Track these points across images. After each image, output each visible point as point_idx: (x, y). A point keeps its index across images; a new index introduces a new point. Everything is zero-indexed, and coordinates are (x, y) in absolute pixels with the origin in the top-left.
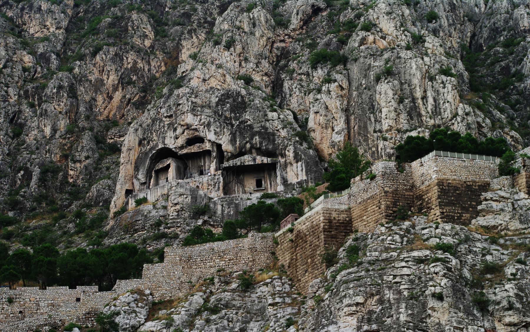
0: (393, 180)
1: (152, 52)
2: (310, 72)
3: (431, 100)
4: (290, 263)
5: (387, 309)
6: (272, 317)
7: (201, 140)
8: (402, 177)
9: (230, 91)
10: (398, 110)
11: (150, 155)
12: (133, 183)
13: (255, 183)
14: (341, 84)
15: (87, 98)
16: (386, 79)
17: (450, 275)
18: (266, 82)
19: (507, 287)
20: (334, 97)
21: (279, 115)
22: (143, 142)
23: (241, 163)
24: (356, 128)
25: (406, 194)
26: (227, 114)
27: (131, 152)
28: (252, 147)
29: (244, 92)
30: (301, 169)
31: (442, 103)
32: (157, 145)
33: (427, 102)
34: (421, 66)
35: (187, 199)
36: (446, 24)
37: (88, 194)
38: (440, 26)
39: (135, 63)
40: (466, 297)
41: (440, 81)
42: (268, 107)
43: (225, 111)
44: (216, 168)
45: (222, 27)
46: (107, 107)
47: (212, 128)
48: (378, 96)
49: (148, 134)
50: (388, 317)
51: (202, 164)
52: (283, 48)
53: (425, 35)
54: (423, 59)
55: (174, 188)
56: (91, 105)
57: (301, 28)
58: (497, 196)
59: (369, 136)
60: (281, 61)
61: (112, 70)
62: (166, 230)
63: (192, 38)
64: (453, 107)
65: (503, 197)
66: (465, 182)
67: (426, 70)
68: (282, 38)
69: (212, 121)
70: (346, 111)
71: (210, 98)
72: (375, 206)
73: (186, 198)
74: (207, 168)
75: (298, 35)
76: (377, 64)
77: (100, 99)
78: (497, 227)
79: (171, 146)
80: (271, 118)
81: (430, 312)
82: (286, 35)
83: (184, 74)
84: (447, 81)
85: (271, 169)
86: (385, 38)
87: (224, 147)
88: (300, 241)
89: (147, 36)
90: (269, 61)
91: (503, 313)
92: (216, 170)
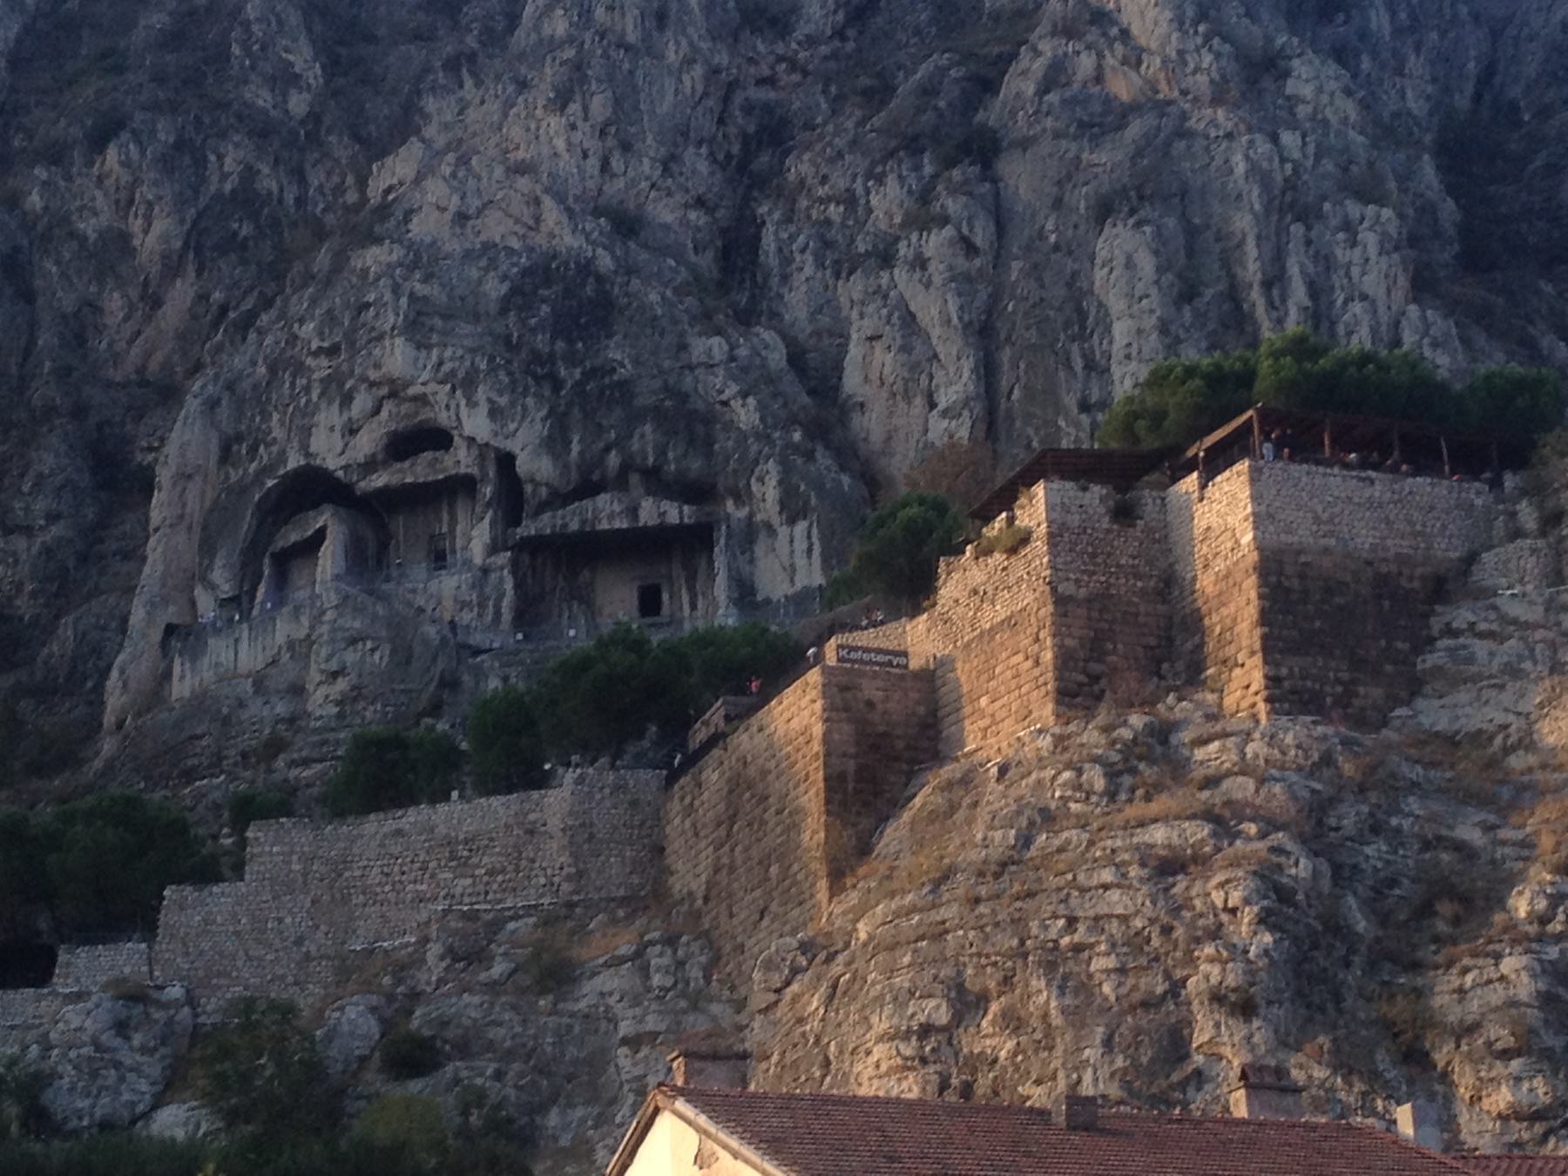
0: (1093, 556)
1: (314, 139)
2: (860, 190)
3: (1299, 293)
4: (710, 885)
5: (1036, 1051)
6: (626, 1088)
7: (439, 439)
8: (1126, 547)
9: (554, 257)
10: (1173, 328)
11: (257, 497)
12: (193, 603)
13: (636, 603)
14: (965, 230)
15: (68, 301)
16: (1132, 212)
17: (1288, 918)
18: (699, 229)
19: (1509, 965)
20: (937, 280)
21: (732, 348)
22: (235, 448)
23: (583, 522)
24: (1016, 394)
25: (1142, 609)
26: (541, 341)
27: (190, 485)
28: (626, 468)
29: (605, 262)
30: (805, 546)
31: (1340, 302)
32: (282, 458)
33: (1284, 300)
34: (1265, 164)
35: (377, 656)
36: (1387, 29)
37: (46, 651)
38: (1364, 35)
39: (249, 173)
40: (1349, 1003)
41: (1334, 222)
42: (693, 320)
43: (533, 331)
44: (494, 540)
45: (547, 31)
46: (139, 333)
47: (481, 393)
48: (1100, 274)
49: (253, 416)
50: (1038, 1082)
51: (445, 529)
52: (768, 108)
53: (1289, 52)
54: (1275, 139)
55: (329, 616)
56: (80, 329)
57: (840, 34)
58: (1493, 616)
59: (1062, 423)
60: (755, 151)
61: (161, 198)
62: (294, 772)
63: (461, 86)
64: (1384, 317)
65: (1515, 622)
66: (1369, 563)
67: (1286, 180)
68: (766, 72)
69: (483, 366)
70: (984, 334)
71: (480, 282)
72: (1020, 657)
73: (373, 650)
74: (459, 543)
75: (826, 58)
76: (1101, 157)
77: (115, 303)
78: (1491, 739)
79: (332, 463)
80: (703, 359)
81: (1199, 1059)
82: (780, 59)
83: (390, 197)
84: (1363, 219)
85: (691, 544)
86: (1139, 62)
87: (523, 465)
88: (748, 795)
89: (297, 77)
90: (711, 154)
91: (1490, 1068)
92: (493, 549)
